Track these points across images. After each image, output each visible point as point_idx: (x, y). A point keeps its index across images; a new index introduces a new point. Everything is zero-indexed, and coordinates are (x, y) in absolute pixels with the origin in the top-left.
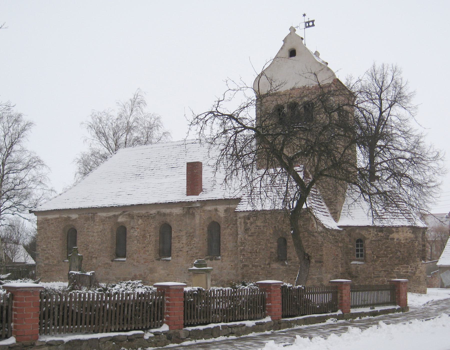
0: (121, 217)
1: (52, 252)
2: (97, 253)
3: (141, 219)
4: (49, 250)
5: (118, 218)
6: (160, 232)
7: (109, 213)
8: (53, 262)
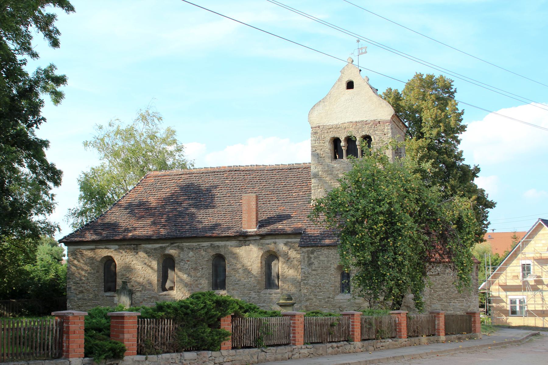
4: (83, 283)
6: (213, 265)
7: (154, 245)
8: (89, 296)
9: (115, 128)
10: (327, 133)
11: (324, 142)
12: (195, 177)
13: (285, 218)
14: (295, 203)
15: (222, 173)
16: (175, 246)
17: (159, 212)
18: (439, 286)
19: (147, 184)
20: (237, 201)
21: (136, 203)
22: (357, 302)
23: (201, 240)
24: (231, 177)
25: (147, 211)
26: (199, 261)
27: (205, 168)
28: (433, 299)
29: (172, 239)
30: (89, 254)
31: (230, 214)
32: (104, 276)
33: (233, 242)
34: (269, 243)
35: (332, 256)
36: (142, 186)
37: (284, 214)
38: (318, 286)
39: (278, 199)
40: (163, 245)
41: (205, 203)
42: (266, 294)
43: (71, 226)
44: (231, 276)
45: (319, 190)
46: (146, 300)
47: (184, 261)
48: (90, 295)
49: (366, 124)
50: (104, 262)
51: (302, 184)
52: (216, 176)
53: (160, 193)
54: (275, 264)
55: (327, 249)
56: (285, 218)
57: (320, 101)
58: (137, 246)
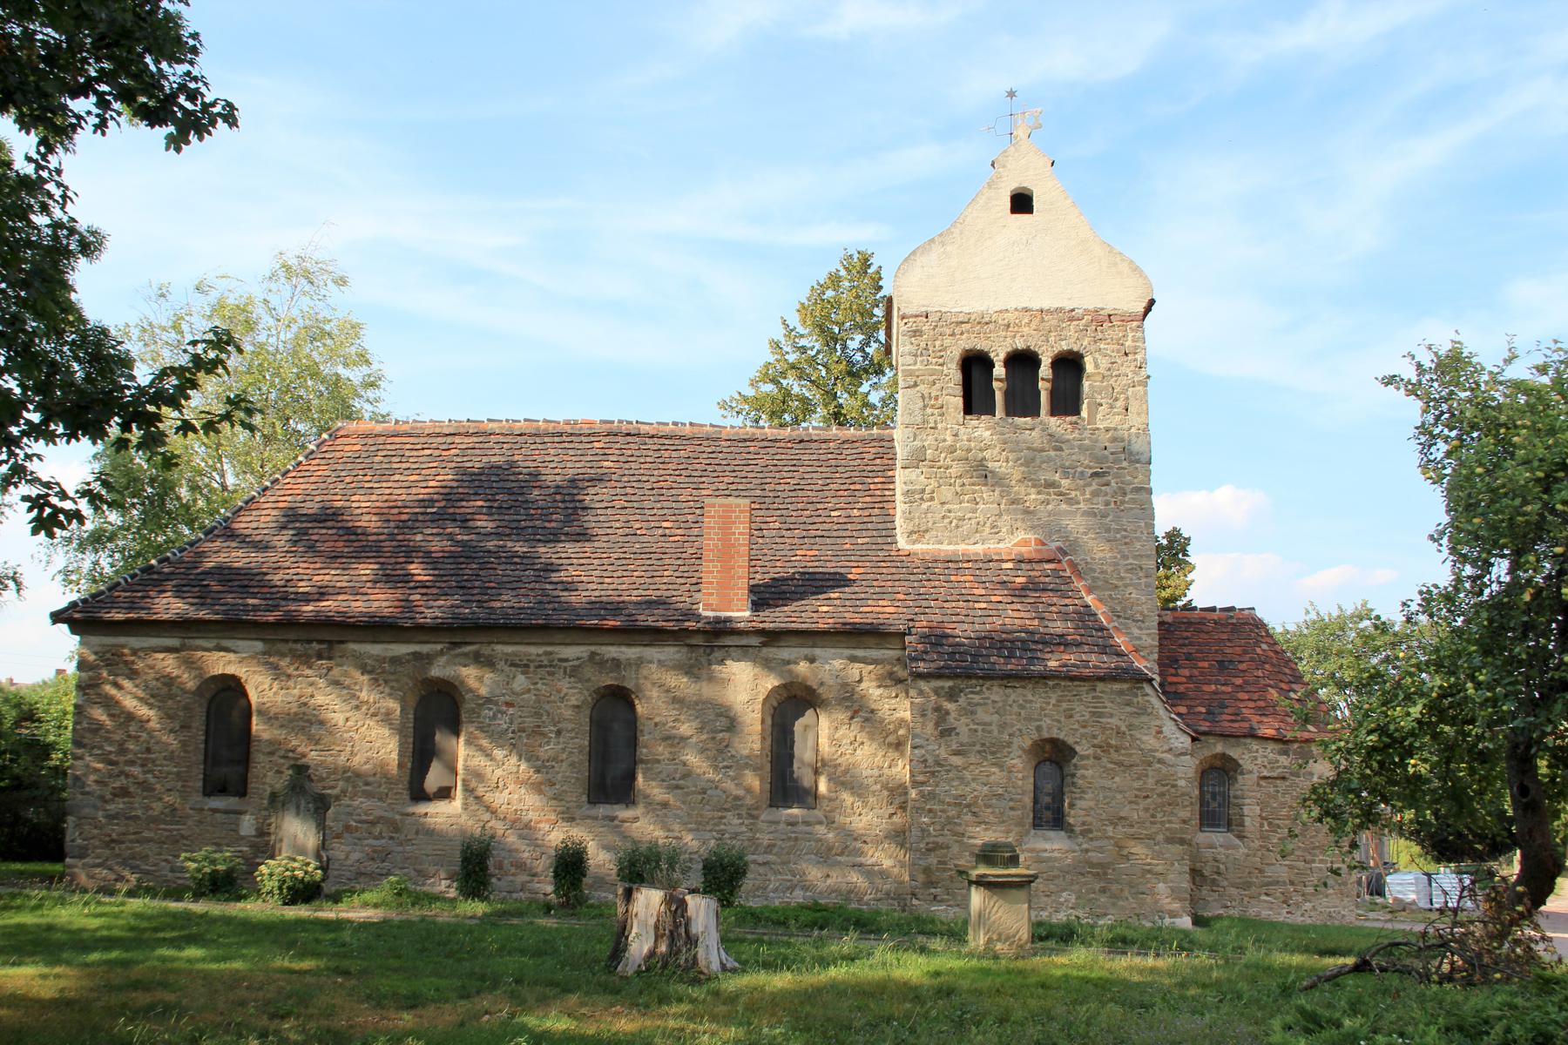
0: (443, 660)
1: (145, 773)
2: (341, 783)
3: (523, 673)
4: (132, 763)
5: (430, 664)
7: (393, 646)
9: (213, 297)
10: (953, 335)
11: (941, 361)
12: (500, 446)
13: (831, 583)
14: (847, 540)
15: (584, 439)
16: (466, 655)
17: (394, 543)
18: (1284, 812)
19: (338, 455)
20: (653, 524)
21: (310, 512)
22: (1095, 861)
23: (559, 637)
24: (617, 452)
25: (353, 537)
26: (547, 707)
27: (526, 420)
28: (1268, 850)
29: (456, 632)
30: (168, 663)
31: (641, 562)
32: (206, 742)
33: (666, 649)
34: (792, 657)
35: (1016, 709)
36: (323, 462)
37: (821, 570)
38: (968, 806)
39: (786, 526)
40: (425, 649)
41: (547, 525)
42: (778, 823)
43: (60, 577)
44: (658, 761)
45: (925, 505)
46: (357, 828)
47: (496, 704)
48: (154, 805)
49: (1071, 319)
50: (208, 695)
51: (852, 487)
52: (566, 445)
53: (390, 485)
54: (806, 727)
55: (1000, 686)
56: (831, 583)
57: (932, 241)
58: (330, 649)
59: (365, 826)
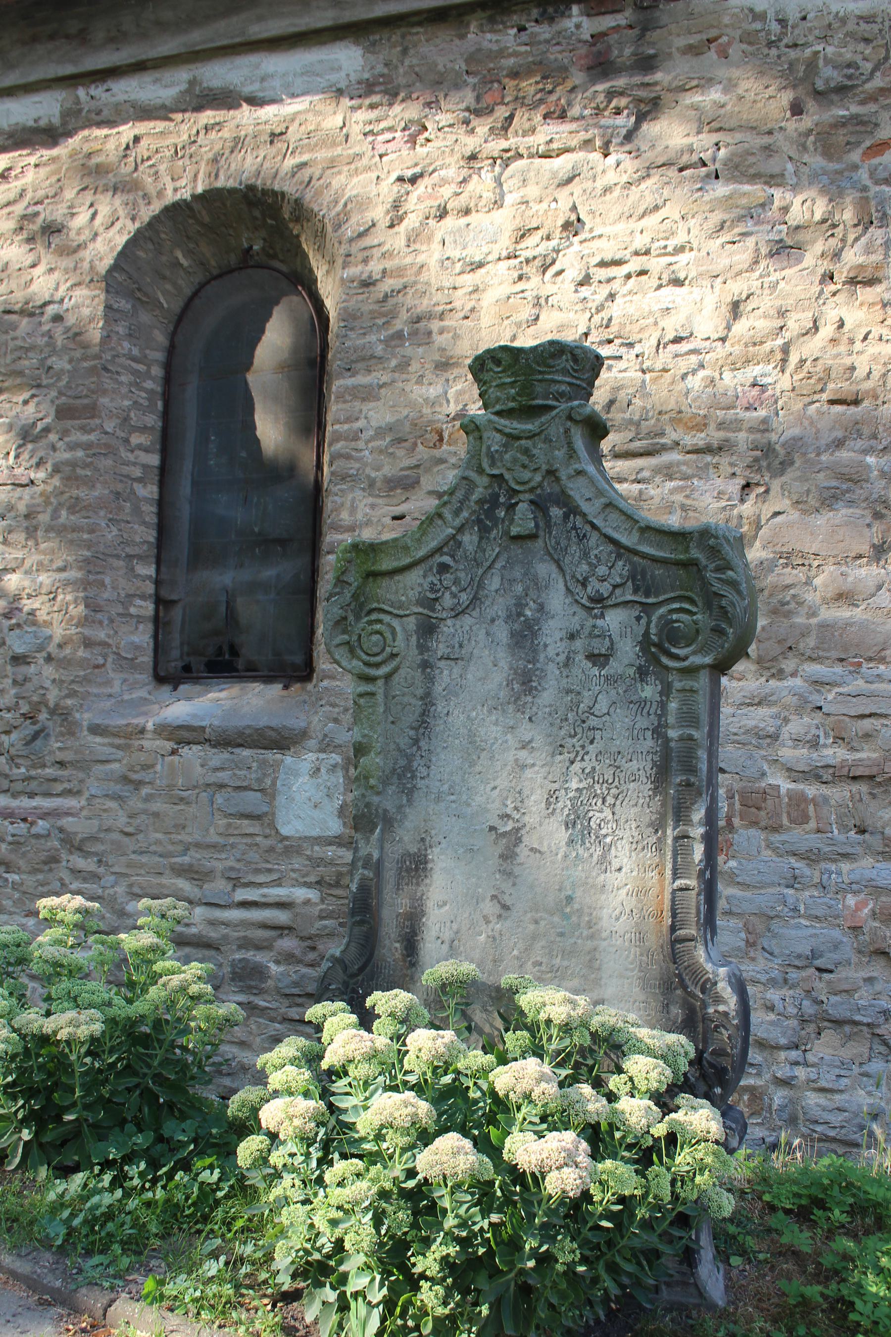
46: (798, 801)
59: (838, 793)
